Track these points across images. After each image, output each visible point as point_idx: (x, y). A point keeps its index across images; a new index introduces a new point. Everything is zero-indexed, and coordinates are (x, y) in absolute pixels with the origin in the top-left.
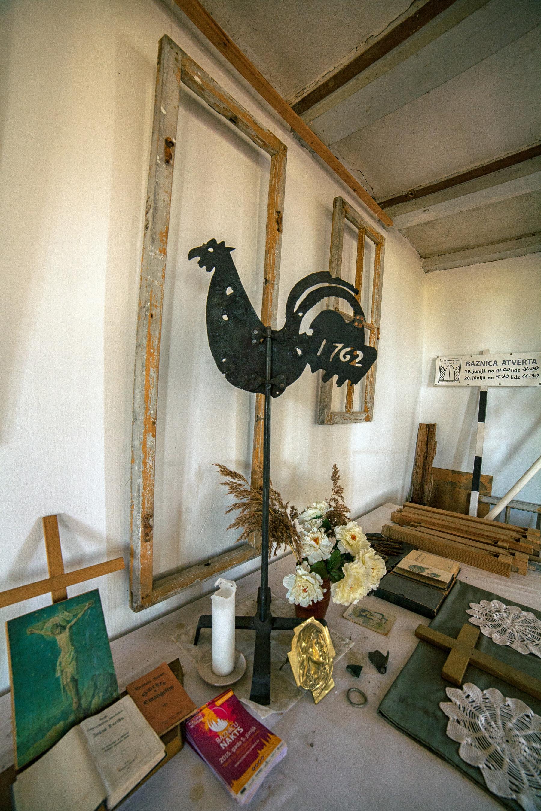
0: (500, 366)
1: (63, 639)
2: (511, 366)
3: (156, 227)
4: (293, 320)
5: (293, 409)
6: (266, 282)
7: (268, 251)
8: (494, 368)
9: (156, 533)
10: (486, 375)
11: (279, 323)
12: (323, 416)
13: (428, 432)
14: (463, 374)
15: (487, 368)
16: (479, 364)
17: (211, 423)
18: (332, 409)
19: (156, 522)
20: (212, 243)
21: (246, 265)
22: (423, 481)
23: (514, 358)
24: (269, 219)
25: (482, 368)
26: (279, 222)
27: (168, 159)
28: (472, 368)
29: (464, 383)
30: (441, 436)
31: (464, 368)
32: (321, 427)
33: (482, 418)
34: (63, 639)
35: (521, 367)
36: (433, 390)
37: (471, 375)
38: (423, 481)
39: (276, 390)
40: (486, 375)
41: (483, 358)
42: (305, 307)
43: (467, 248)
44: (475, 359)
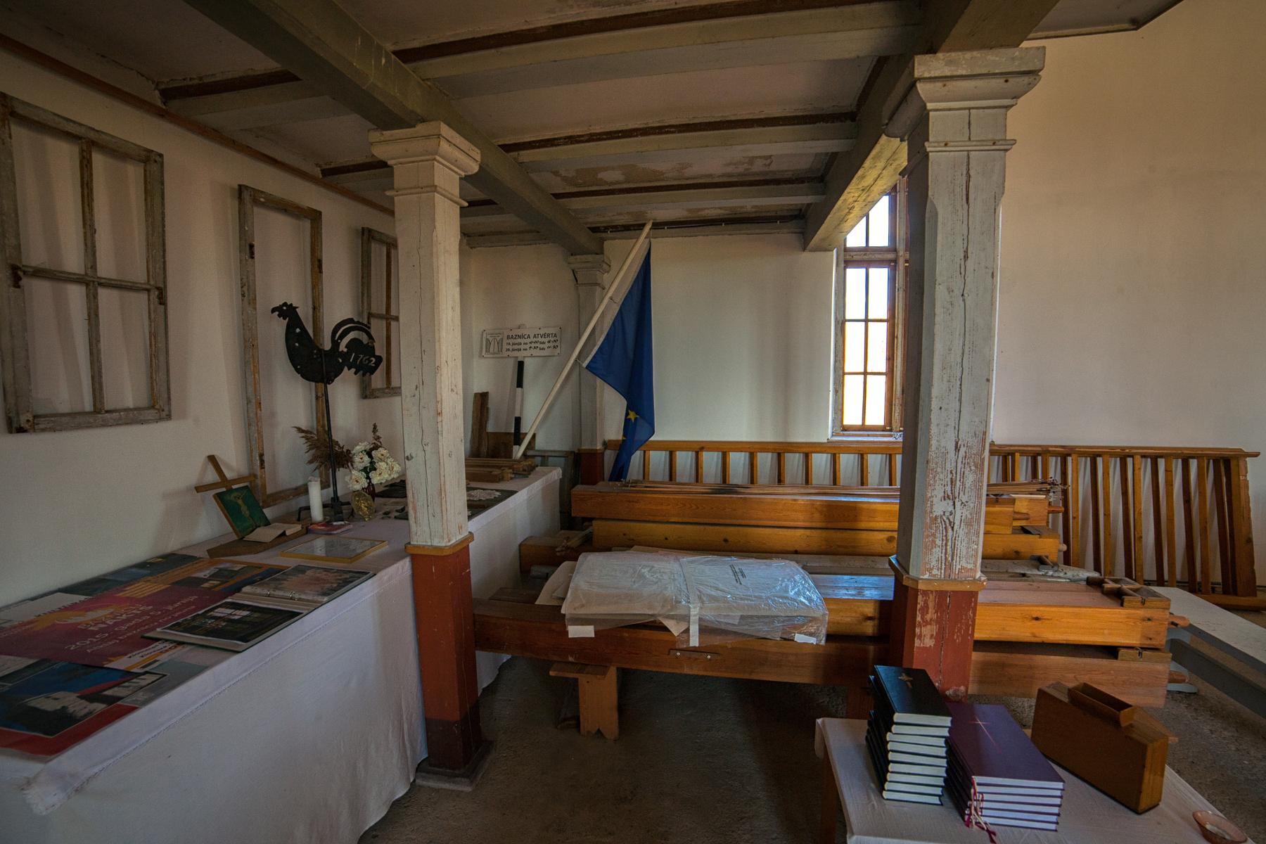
0: (532, 339)
1: (240, 502)
2: (540, 339)
3: (247, 292)
4: (335, 344)
5: (344, 391)
6: (314, 308)
7: (313, 288)
8: (528, 341)
9: (266, 464)
10: (522, 347)
11: (327, 346)
12: (366, 393)
13: (482, 400)
14: (505, 347)
15: (522, 341)
16: (515, 338)
17: (291, 401)
18: (373, 386)
19: (265, 458)
20: (285, 304)
21: (304, 312)
22: (480, 444)
23: (542, 332)
24: (312, 264)
25: (519, 340)
26: (320, 267)
27: (252, 256)
28: (511, 341)
29: (506, 354)
30: (492, 404)
31: (506, 341)
32: (366, 401)
33: (520, 384)
34: (240, 502)
35: (546, 340)
36: (483, 361)
37: (510, 347)
38: (480, 444)
39: (329, 380)
40: (522, 347)
41: (519, 332)
42: (342, 337)
43: (501, 233)
44: (514, 333)
